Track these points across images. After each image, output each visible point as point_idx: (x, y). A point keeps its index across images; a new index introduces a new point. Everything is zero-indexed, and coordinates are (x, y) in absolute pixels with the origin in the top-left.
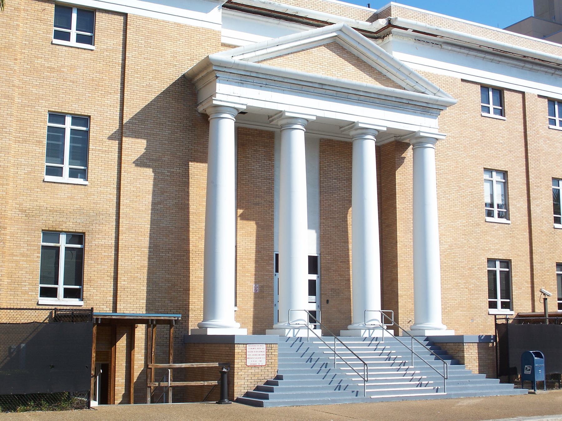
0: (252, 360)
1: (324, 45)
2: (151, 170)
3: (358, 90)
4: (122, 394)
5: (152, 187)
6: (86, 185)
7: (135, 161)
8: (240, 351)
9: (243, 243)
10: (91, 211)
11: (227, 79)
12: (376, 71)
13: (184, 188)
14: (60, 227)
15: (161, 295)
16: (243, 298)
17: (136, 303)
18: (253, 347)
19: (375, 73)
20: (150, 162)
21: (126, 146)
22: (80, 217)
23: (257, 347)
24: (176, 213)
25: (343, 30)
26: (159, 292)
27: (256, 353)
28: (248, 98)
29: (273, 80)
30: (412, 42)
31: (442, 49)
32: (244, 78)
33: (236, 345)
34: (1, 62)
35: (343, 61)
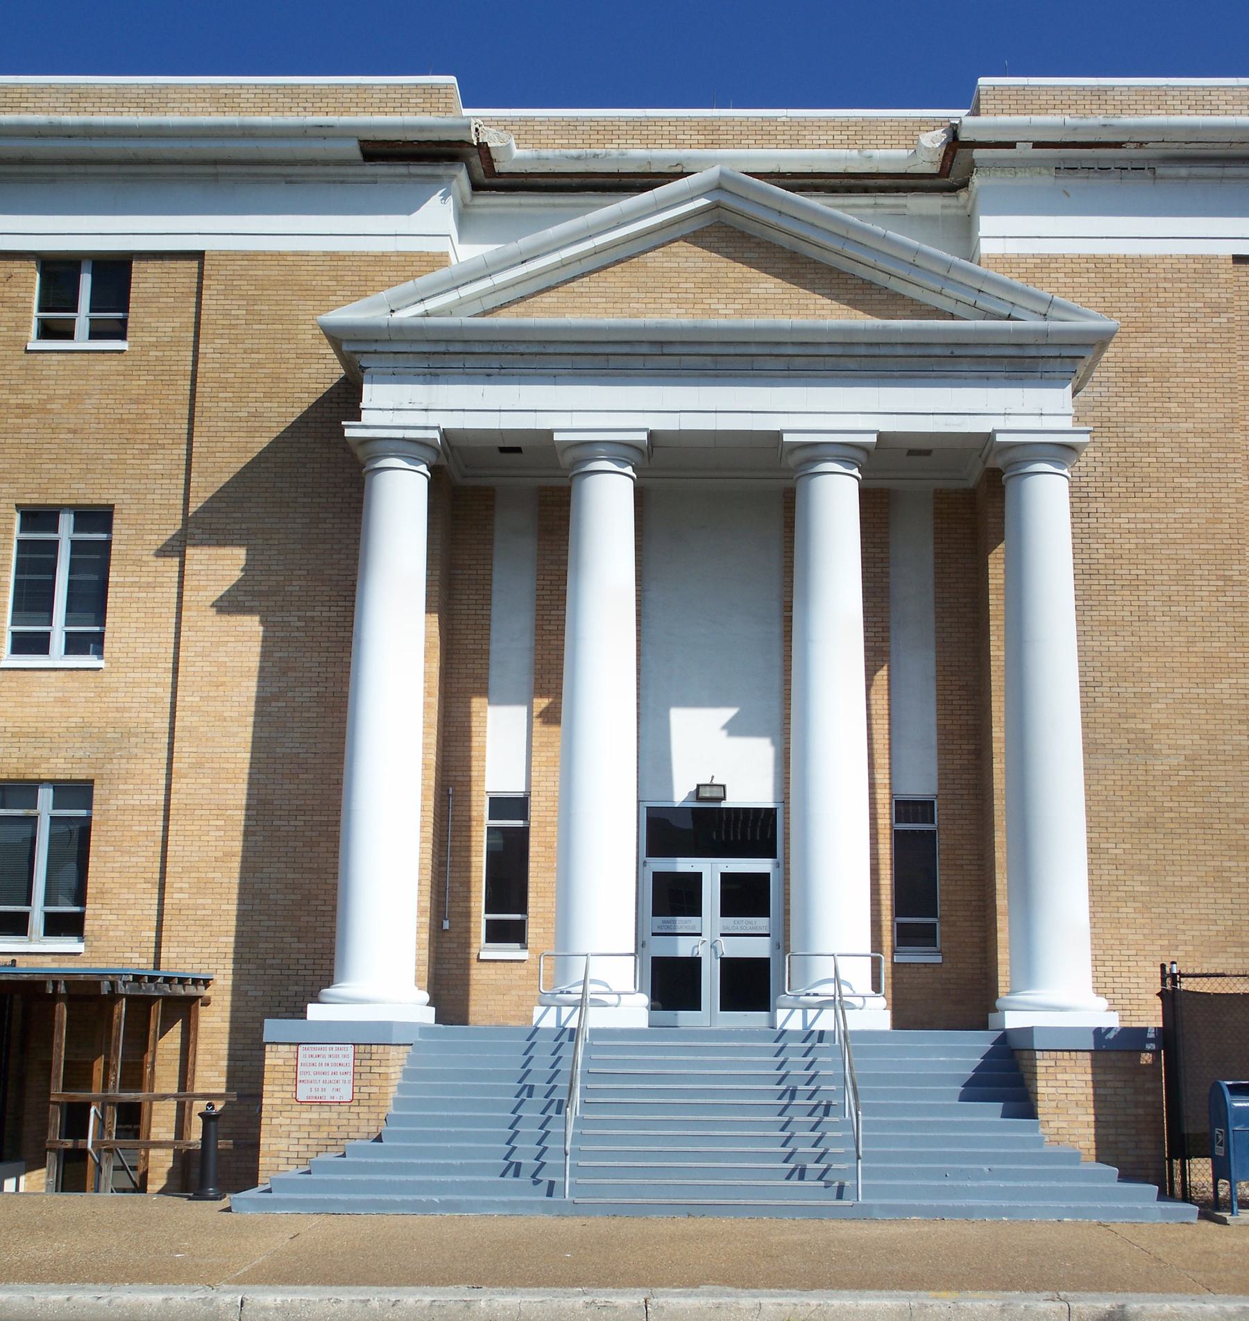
0: (313, 1086)
1: (685, 238)
2: (257, 618)
3: (778, 344)
4: (165, 1170)
5: (258, 659)
6: (98, 669)
8: (280, 1062)
9: (548, 784)
10: (109, 730)
11: (391, 370)
12: (855, 282)
14: (35, 771)
15: (273, 923)
16: (546, 926)
18: (315, 1053)
19: (850, 287)
21: (195, 567)
22: (83, 745)
23: (327, 1053)
24: (317, 720)
26: (269, 915)
27: (324, 1069)
28: (452, 410)
29: (517, 354)
30: (1046, 179)
31: (1157, 181)
32: (435, 362)
33: (268, 1047)
35: (745, 269)
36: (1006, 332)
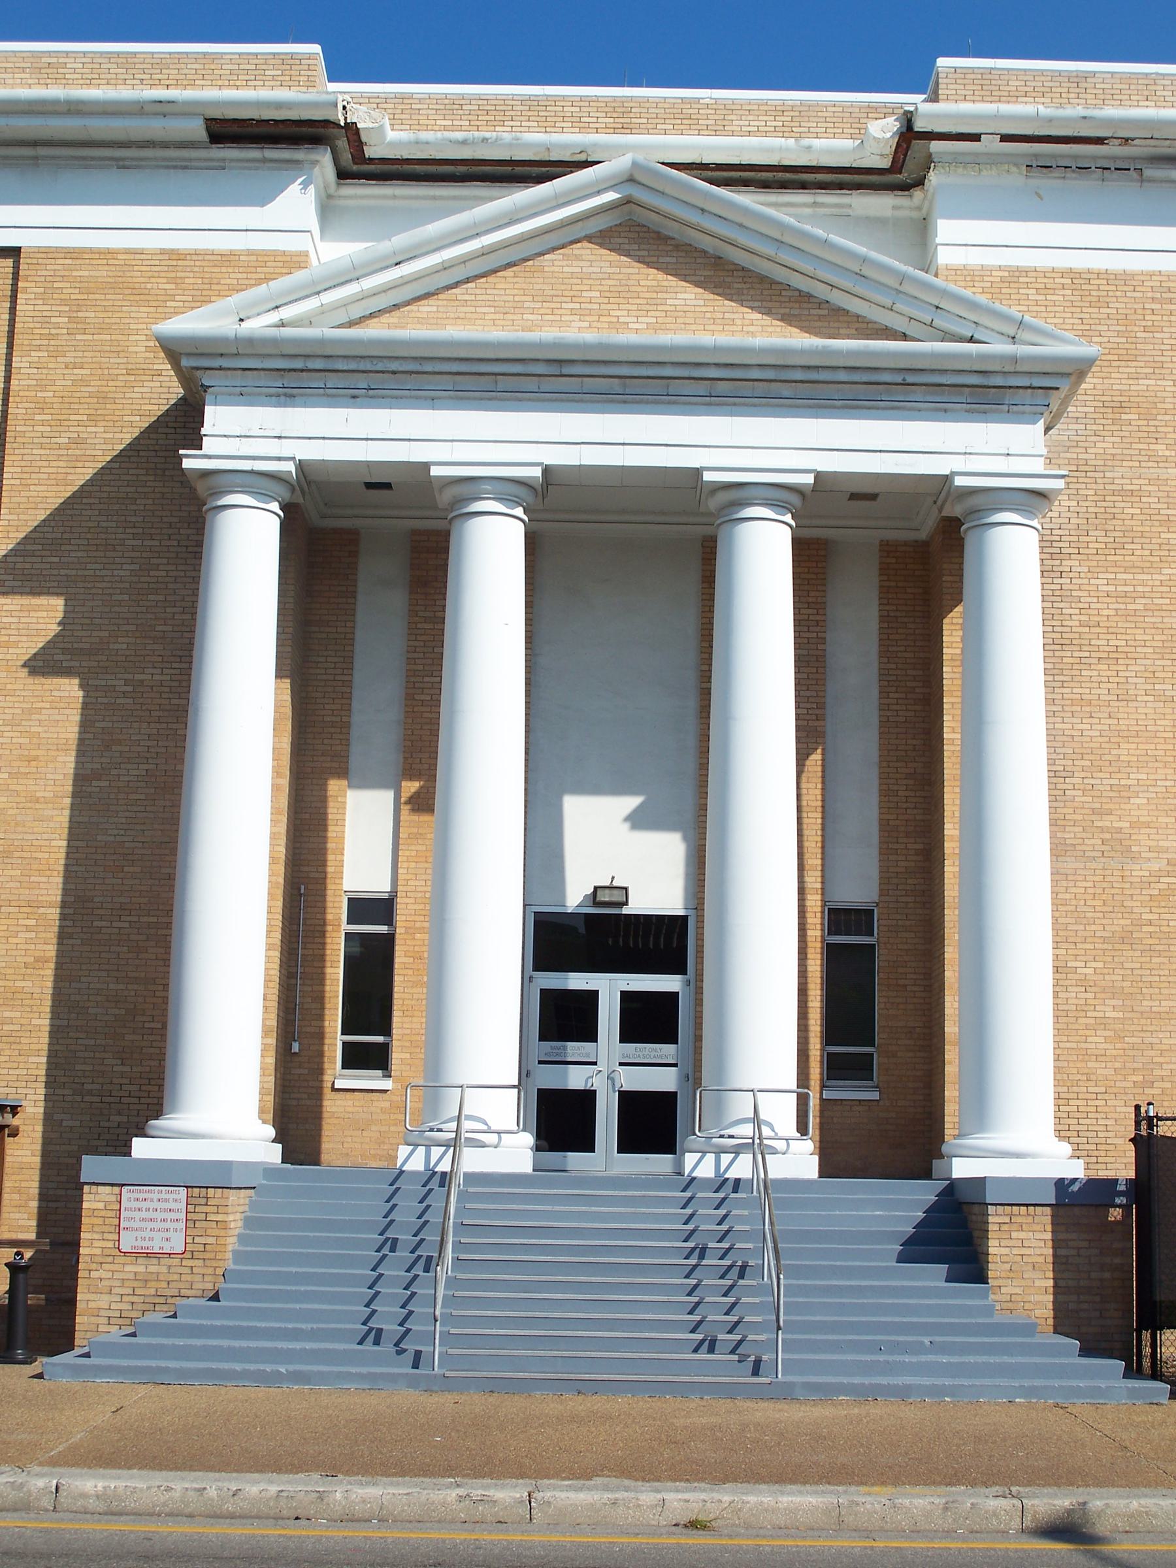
0: (140, 1234)
1: (589, 238)
2: (76, 681)
7: (29, 660)
8: (101, 1205)
9: (417, 883)
11: (238, 390)
13: (174, 726)
16: (413, 1050)
17: (15, 1065)
19: (783, 299)
20: (71, 660)
23: (156, 1196)
25: (638, 177)
28: (310, 438)
30: (1016, 178)
31: (1145, 184)
34: (1173, 453)
36: (968, 356)
